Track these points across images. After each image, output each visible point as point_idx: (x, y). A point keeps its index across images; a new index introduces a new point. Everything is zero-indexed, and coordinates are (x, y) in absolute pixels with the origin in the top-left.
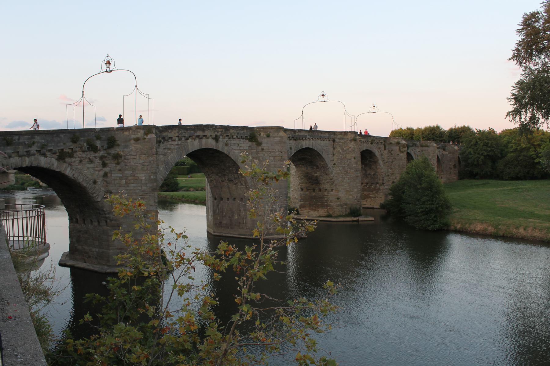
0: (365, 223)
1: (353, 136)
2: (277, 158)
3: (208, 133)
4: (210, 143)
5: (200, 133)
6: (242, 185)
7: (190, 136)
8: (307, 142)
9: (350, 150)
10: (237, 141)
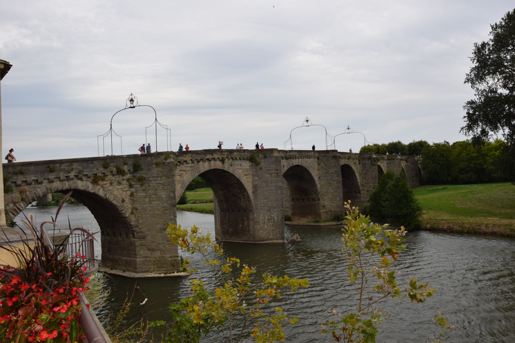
5: (209, 156)
9: (332, 165)
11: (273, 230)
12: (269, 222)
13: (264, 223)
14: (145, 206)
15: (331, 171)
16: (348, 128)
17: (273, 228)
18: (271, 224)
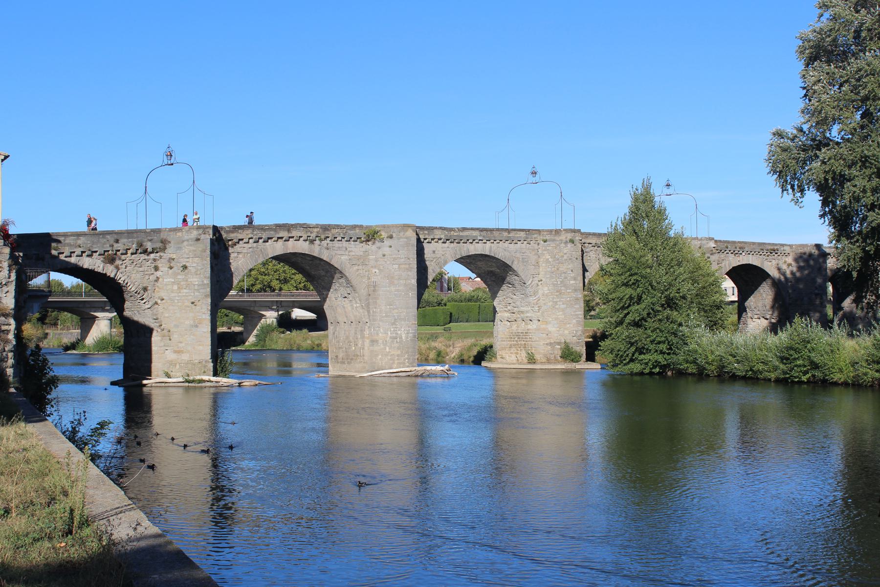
0: (508, 371)
1: (569, 236)
2: (403, 266)
3: (295, 233)
4: (301, 247)
5: (284, 234)
6: (356, 303)
7: (269, 238)
8: (480, 245)
9: (565, 257)
10: (344, 244)
11: (398, 356)
12: (393, 342)
13: (385, 343)
14: (173, 295)
15: (563, 268)
16: (668, 185)
17: (399, 352)
18: (397, 345)
